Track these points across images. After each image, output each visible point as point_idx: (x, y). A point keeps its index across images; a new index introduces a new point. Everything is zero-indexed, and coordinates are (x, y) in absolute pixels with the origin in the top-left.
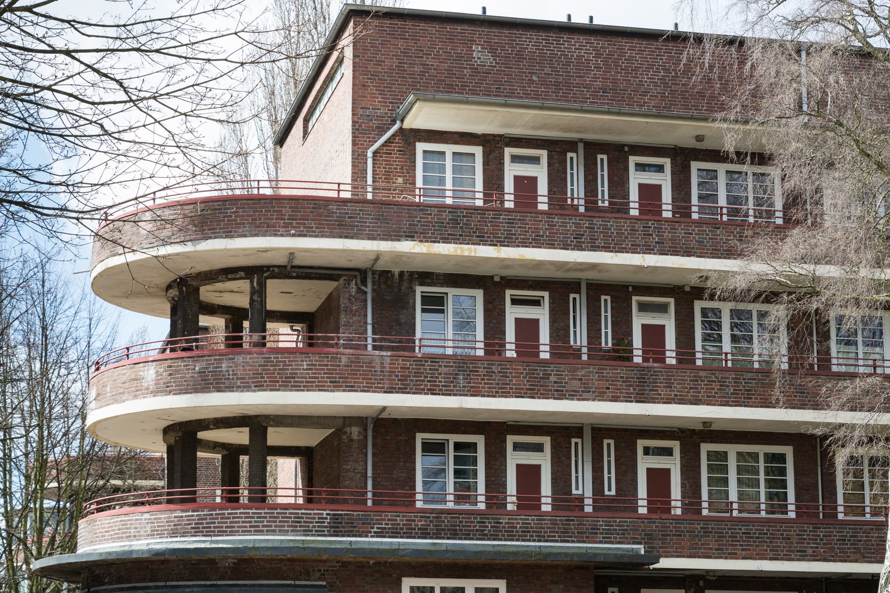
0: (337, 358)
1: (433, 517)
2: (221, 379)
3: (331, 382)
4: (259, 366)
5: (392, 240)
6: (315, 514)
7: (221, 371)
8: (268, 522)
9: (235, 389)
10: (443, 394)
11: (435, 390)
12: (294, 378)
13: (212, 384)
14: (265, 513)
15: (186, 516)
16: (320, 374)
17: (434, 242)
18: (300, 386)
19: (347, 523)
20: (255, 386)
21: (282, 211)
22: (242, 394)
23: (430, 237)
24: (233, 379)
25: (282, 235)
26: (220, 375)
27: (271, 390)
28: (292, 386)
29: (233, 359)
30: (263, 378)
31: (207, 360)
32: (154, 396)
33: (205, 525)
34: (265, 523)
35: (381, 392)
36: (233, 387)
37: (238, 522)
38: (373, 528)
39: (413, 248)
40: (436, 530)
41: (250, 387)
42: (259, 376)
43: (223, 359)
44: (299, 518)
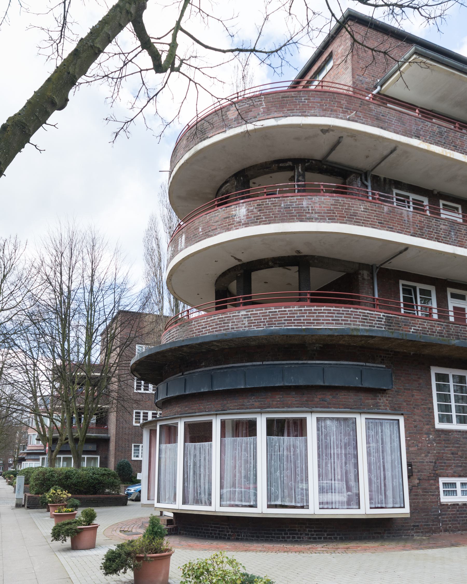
0: (381, 207)
1: (445, 325)
2: (303, 213)
3: (379, 223)
4: (331, 205)
5: (408, 136)
6: (375, 314)
7: (303, 207)
8: (345, 317)
9: (314, 220)
10: (444, 243)
11: (439, 239)
12: (356, 216)
13: (295, 216)
14: (342, 311)
15: (279, 311)
16: (372, 216)
17: (431, 143)
18: (360, 222)
19: (395, 323)
20: (329, 219)
21: (340, 102)
22: (319, 224)
23: (428, 140)
24: (312, 213)
25: (341, 118)
26: (302, 210)
27: (341, 223)
28: (355, 222)
29: (312, 199)
30: (335, 213)
31: (291, 200)
32: (246, 227)
33: (296, 318)
34: (343, 318)
35: (408, 235)
36: (312, 219)
37: (323, 316)
38: (411, 329)
39: (420, 144)
40: (448, 334)
41: (325, 219)
42: (332, 212)
43: (303, 199)
44: (366, 316)
